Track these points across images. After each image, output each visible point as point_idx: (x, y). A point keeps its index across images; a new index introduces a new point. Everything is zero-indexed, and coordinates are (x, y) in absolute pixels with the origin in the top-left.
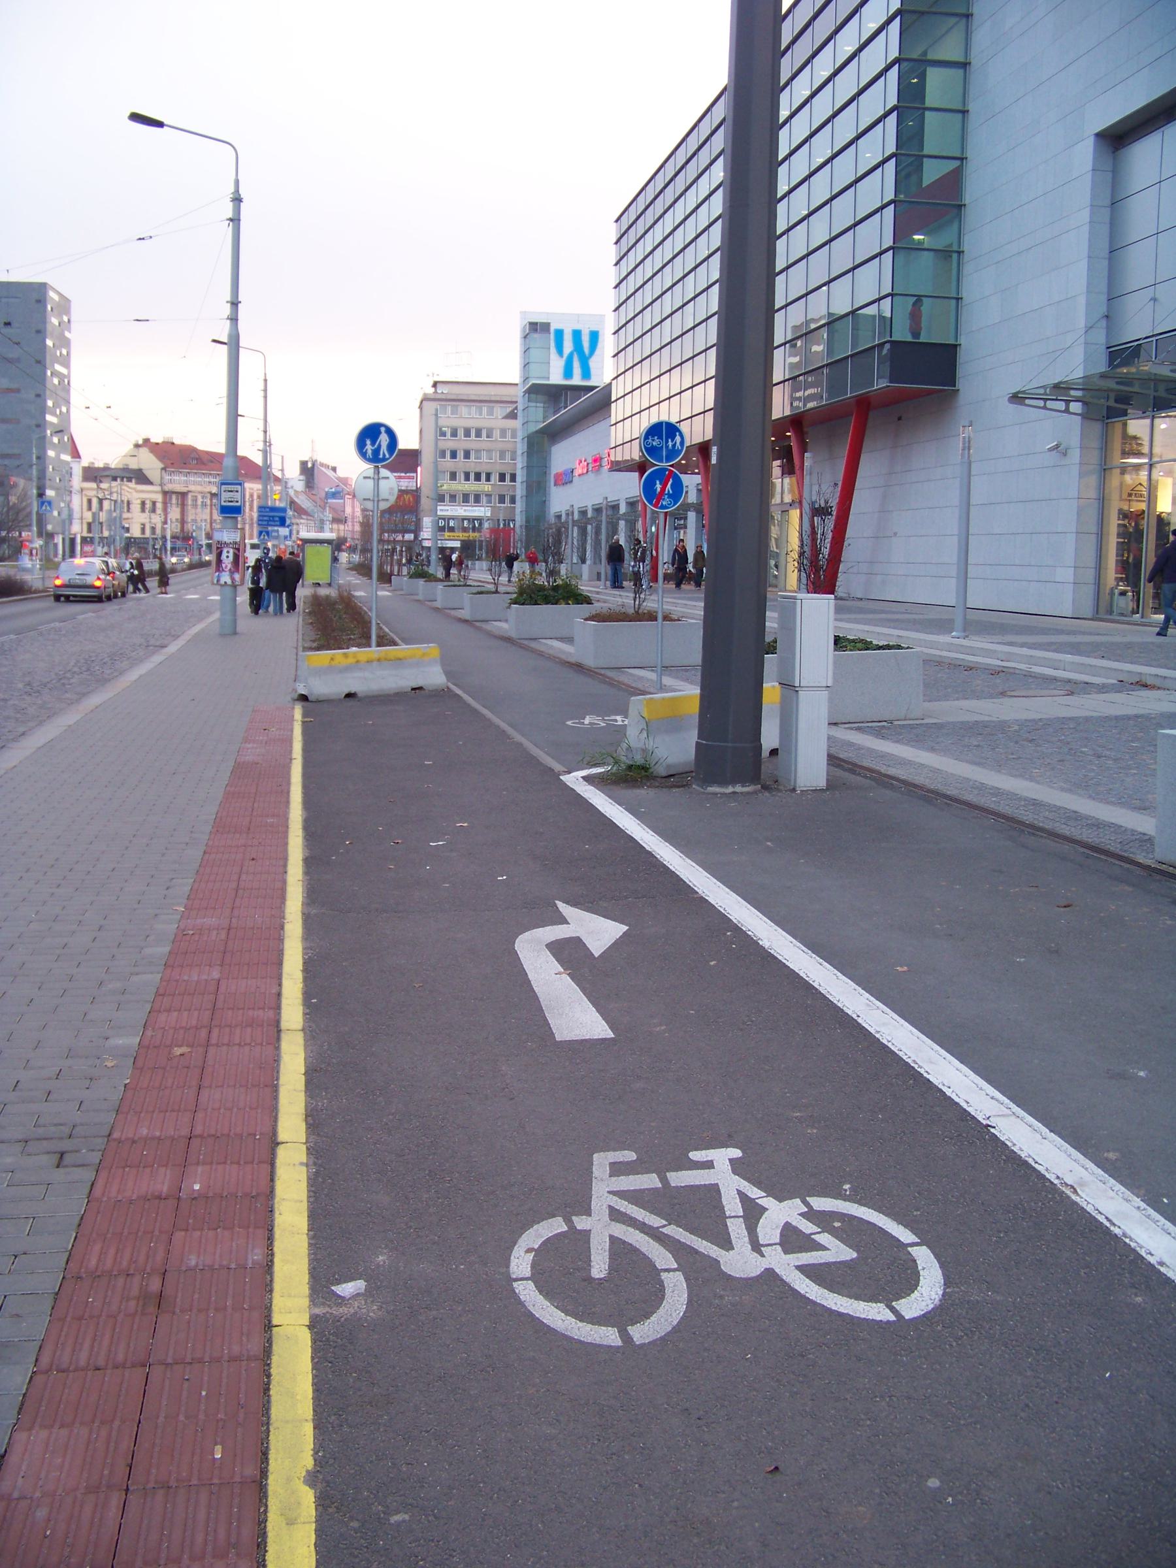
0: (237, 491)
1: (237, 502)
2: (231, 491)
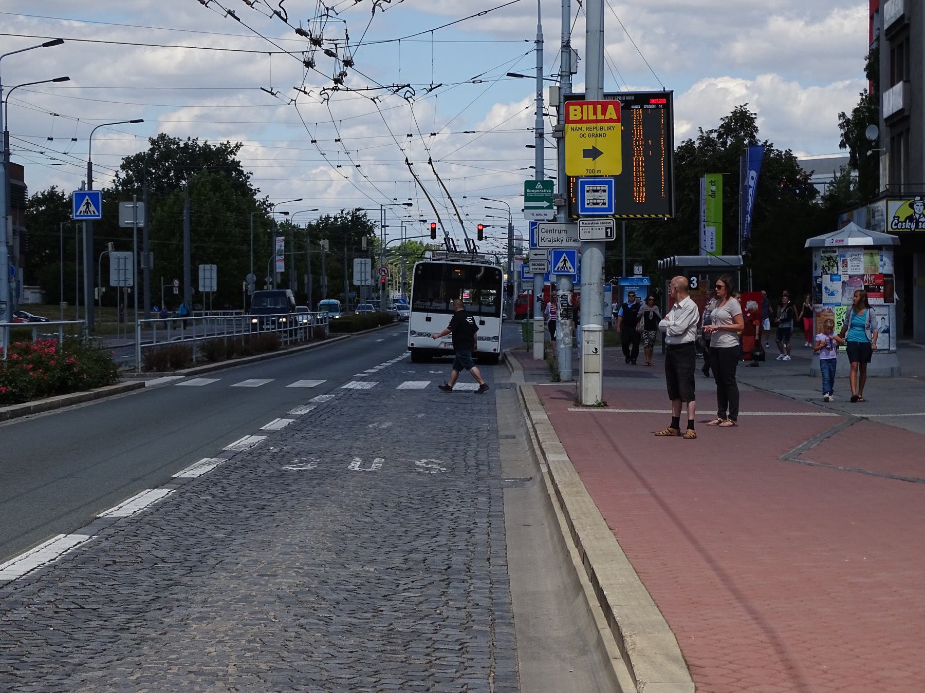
0: (604, 191)
1: (604, 204)
2: (597, 191)
